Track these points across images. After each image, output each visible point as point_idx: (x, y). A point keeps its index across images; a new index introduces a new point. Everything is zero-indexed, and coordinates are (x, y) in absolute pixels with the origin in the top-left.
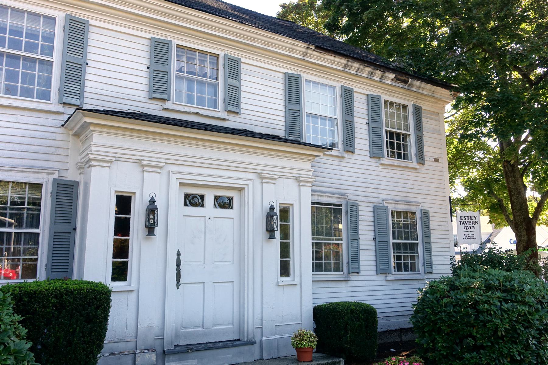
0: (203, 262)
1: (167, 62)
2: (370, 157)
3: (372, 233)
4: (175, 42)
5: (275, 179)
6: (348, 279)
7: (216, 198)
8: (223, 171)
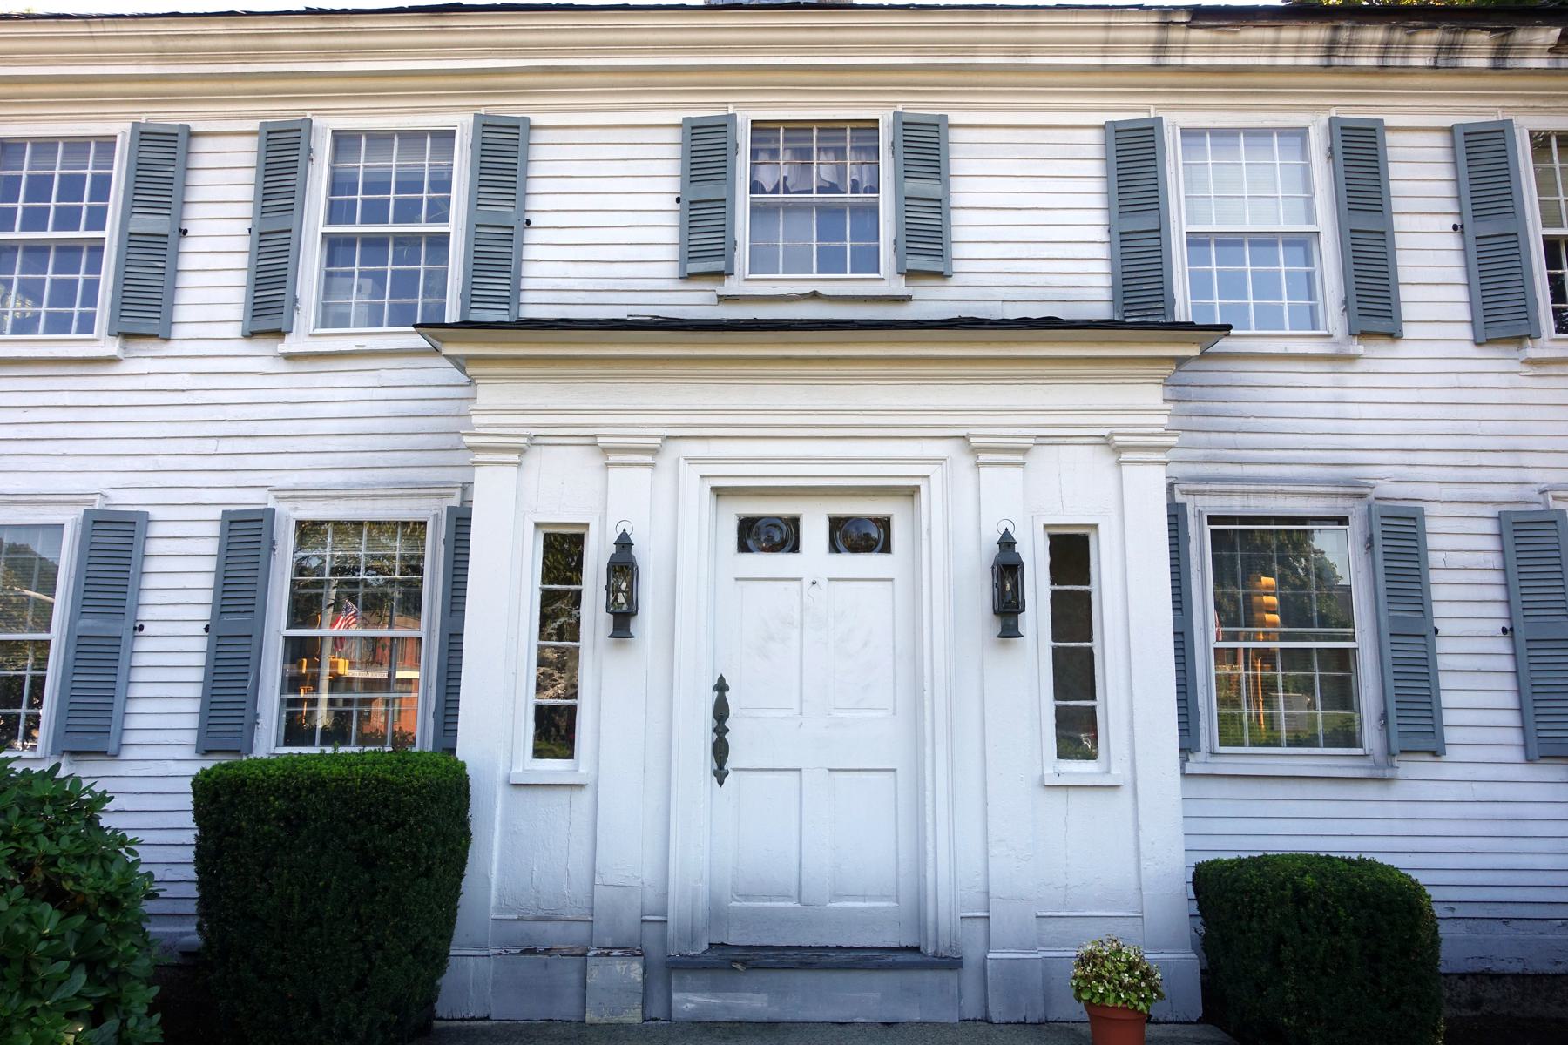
0: (797, 711)
1: (724, 174)
2: (1478, 344)
3: (1499, 611)
4: (745, 118)
5: (1025, 451)
6: (1388, 773)
7: (836, 524)
8: (904, 442)
